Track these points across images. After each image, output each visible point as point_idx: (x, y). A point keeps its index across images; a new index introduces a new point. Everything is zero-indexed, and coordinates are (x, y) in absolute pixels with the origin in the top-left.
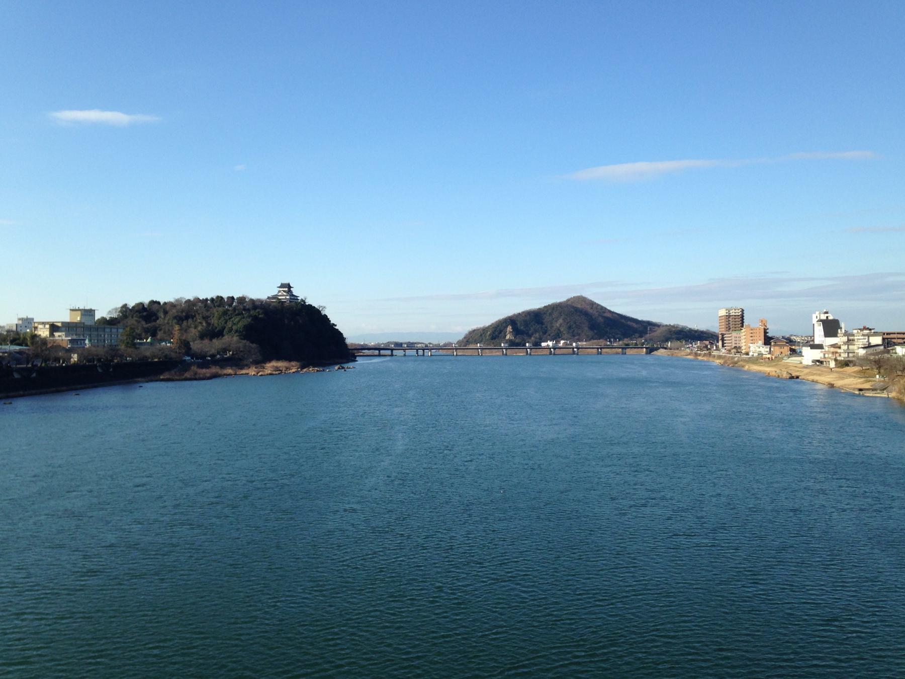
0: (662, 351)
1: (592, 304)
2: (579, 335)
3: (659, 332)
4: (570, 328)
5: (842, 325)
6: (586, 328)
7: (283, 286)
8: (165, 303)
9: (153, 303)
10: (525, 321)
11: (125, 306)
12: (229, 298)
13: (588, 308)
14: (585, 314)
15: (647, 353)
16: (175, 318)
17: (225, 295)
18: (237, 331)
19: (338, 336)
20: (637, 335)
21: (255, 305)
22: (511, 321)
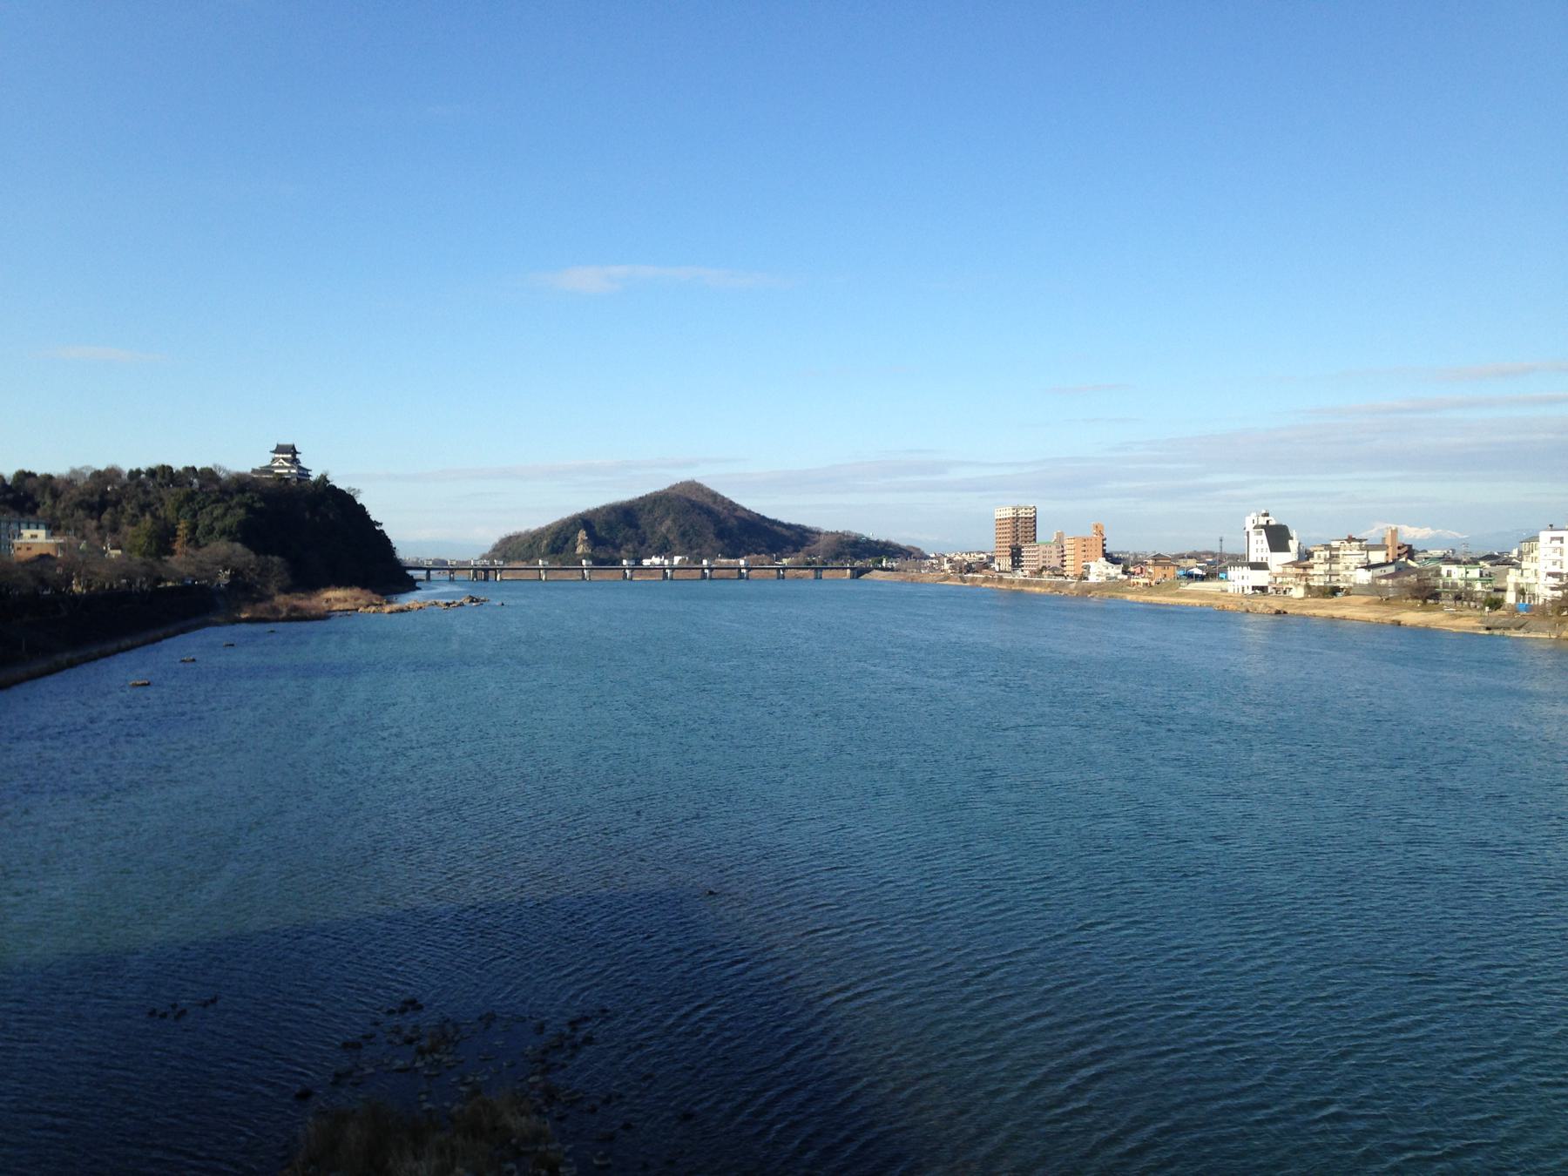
0: (877, 575)
1: (715, 496)
2: (700, 547)
3: (823, 543)
4: (684, 534)
5: (1293, 533)
6: (711, 536)
7: (280, 449)
9: (23, 476)
10: (607, 523)
12: (131, 473)
13: (709, 501)
14: (709, 512)
15: (852, 577)
16: (79, 505)
17: (178, 465)
18: (223, 533)
19: (379, 543)
20: (790, 548)
21: (243, 484)
22: (584, 522)
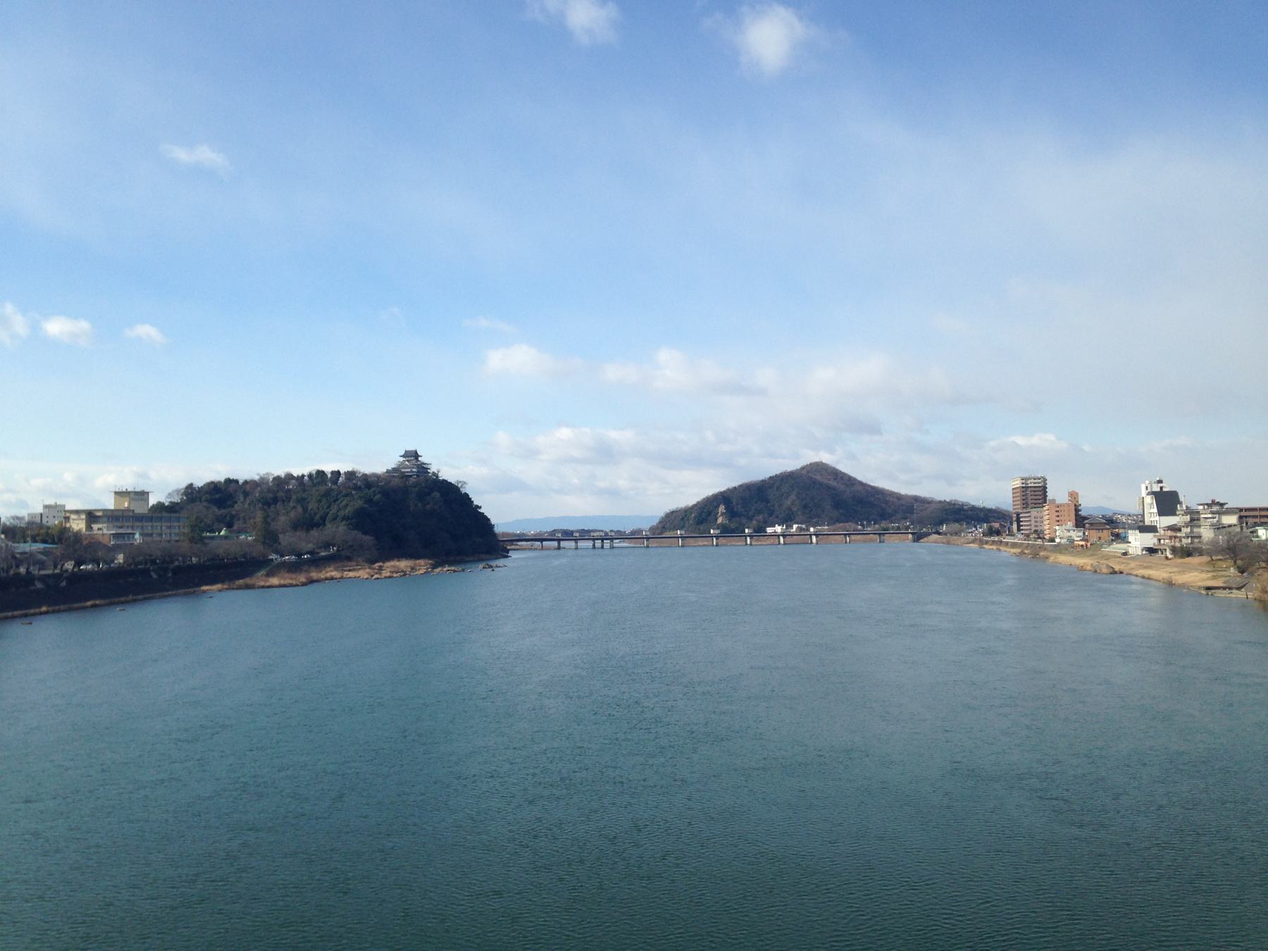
4: (805, 507)
9: (229, 481)
11: (191, 485)
12: (333, 473)
18: (344, 519)
19: (482, 523)
22: (723, 498)
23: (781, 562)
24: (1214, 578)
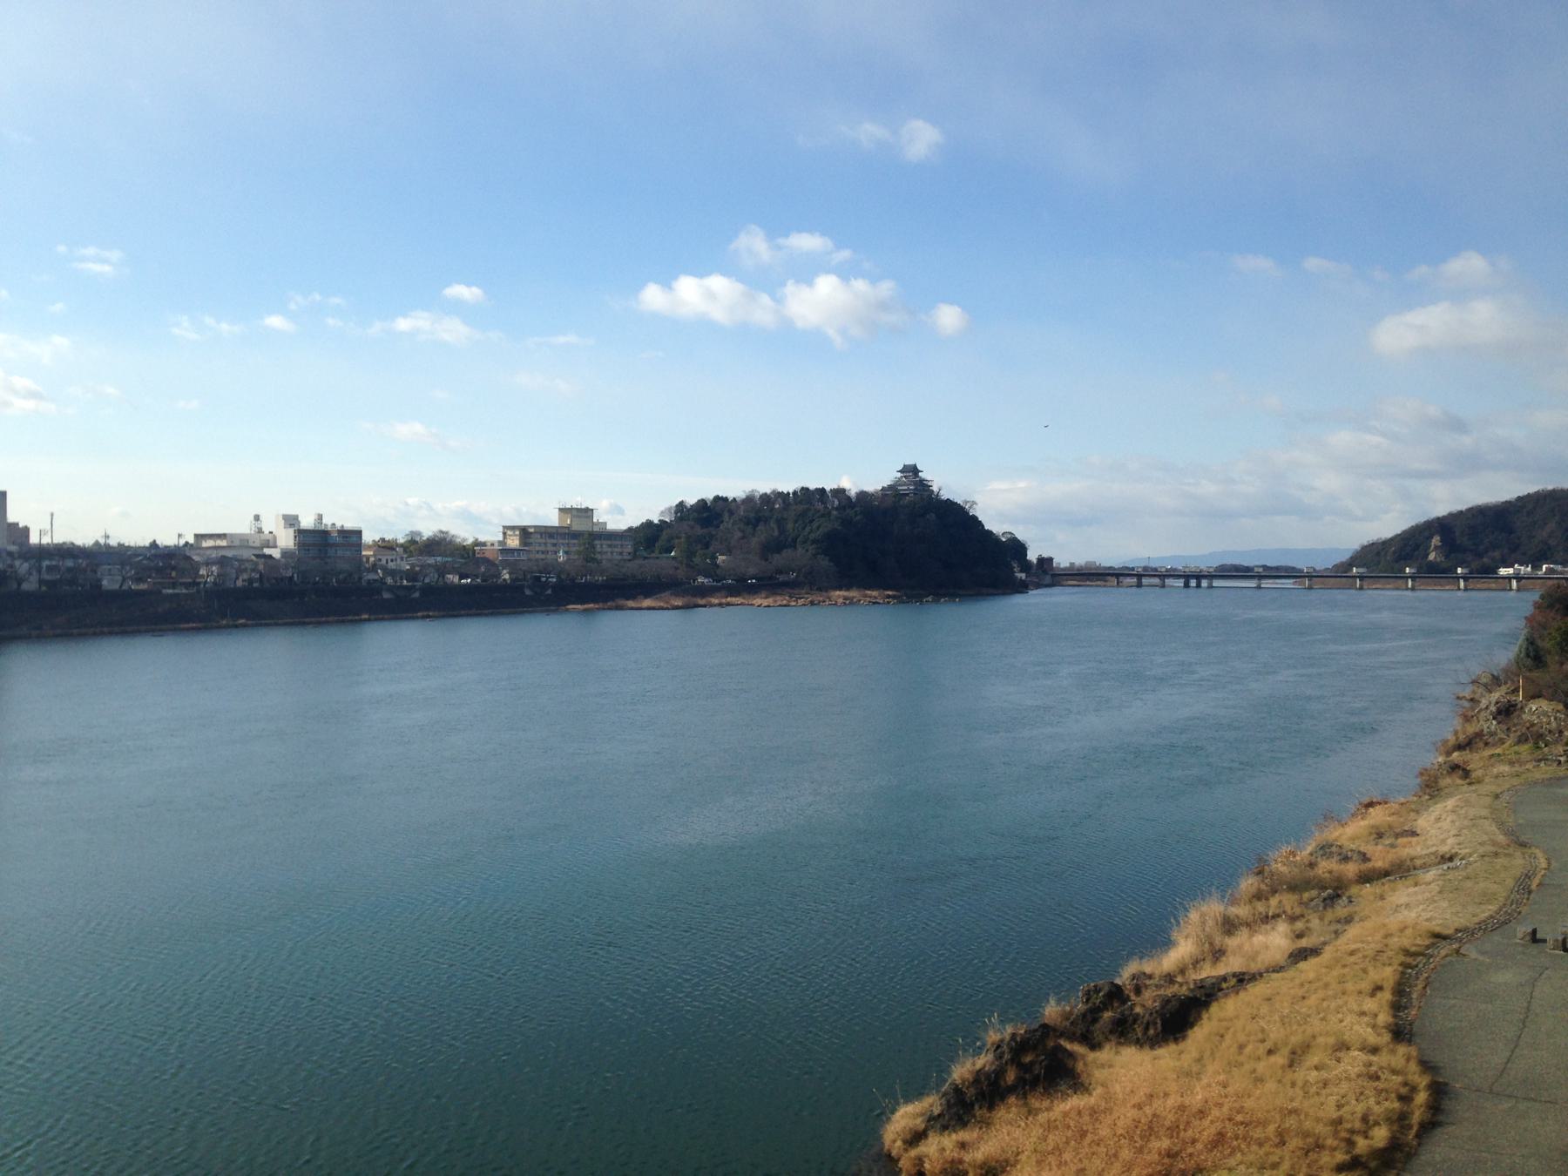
1: (438, 545)
8: (795, 493)
9: (717, 499)
11: (681, 503)
18: (814, 541)
22: (1443, 527)
23: (840, 643)
24: (1071, 1055)
